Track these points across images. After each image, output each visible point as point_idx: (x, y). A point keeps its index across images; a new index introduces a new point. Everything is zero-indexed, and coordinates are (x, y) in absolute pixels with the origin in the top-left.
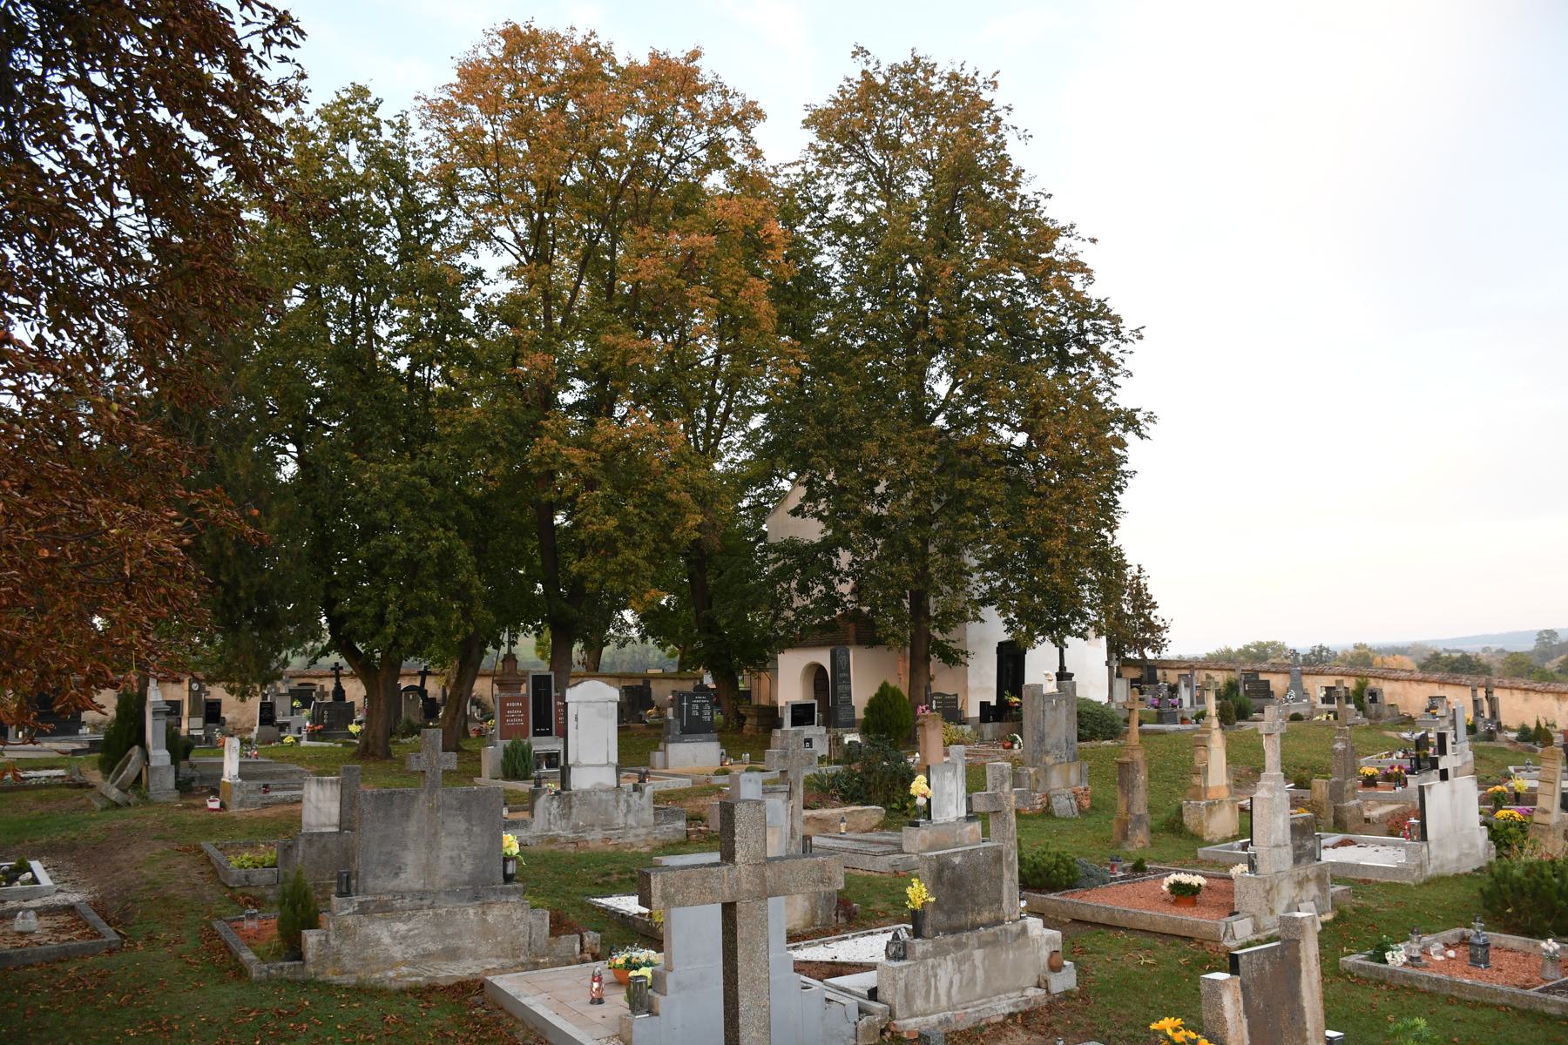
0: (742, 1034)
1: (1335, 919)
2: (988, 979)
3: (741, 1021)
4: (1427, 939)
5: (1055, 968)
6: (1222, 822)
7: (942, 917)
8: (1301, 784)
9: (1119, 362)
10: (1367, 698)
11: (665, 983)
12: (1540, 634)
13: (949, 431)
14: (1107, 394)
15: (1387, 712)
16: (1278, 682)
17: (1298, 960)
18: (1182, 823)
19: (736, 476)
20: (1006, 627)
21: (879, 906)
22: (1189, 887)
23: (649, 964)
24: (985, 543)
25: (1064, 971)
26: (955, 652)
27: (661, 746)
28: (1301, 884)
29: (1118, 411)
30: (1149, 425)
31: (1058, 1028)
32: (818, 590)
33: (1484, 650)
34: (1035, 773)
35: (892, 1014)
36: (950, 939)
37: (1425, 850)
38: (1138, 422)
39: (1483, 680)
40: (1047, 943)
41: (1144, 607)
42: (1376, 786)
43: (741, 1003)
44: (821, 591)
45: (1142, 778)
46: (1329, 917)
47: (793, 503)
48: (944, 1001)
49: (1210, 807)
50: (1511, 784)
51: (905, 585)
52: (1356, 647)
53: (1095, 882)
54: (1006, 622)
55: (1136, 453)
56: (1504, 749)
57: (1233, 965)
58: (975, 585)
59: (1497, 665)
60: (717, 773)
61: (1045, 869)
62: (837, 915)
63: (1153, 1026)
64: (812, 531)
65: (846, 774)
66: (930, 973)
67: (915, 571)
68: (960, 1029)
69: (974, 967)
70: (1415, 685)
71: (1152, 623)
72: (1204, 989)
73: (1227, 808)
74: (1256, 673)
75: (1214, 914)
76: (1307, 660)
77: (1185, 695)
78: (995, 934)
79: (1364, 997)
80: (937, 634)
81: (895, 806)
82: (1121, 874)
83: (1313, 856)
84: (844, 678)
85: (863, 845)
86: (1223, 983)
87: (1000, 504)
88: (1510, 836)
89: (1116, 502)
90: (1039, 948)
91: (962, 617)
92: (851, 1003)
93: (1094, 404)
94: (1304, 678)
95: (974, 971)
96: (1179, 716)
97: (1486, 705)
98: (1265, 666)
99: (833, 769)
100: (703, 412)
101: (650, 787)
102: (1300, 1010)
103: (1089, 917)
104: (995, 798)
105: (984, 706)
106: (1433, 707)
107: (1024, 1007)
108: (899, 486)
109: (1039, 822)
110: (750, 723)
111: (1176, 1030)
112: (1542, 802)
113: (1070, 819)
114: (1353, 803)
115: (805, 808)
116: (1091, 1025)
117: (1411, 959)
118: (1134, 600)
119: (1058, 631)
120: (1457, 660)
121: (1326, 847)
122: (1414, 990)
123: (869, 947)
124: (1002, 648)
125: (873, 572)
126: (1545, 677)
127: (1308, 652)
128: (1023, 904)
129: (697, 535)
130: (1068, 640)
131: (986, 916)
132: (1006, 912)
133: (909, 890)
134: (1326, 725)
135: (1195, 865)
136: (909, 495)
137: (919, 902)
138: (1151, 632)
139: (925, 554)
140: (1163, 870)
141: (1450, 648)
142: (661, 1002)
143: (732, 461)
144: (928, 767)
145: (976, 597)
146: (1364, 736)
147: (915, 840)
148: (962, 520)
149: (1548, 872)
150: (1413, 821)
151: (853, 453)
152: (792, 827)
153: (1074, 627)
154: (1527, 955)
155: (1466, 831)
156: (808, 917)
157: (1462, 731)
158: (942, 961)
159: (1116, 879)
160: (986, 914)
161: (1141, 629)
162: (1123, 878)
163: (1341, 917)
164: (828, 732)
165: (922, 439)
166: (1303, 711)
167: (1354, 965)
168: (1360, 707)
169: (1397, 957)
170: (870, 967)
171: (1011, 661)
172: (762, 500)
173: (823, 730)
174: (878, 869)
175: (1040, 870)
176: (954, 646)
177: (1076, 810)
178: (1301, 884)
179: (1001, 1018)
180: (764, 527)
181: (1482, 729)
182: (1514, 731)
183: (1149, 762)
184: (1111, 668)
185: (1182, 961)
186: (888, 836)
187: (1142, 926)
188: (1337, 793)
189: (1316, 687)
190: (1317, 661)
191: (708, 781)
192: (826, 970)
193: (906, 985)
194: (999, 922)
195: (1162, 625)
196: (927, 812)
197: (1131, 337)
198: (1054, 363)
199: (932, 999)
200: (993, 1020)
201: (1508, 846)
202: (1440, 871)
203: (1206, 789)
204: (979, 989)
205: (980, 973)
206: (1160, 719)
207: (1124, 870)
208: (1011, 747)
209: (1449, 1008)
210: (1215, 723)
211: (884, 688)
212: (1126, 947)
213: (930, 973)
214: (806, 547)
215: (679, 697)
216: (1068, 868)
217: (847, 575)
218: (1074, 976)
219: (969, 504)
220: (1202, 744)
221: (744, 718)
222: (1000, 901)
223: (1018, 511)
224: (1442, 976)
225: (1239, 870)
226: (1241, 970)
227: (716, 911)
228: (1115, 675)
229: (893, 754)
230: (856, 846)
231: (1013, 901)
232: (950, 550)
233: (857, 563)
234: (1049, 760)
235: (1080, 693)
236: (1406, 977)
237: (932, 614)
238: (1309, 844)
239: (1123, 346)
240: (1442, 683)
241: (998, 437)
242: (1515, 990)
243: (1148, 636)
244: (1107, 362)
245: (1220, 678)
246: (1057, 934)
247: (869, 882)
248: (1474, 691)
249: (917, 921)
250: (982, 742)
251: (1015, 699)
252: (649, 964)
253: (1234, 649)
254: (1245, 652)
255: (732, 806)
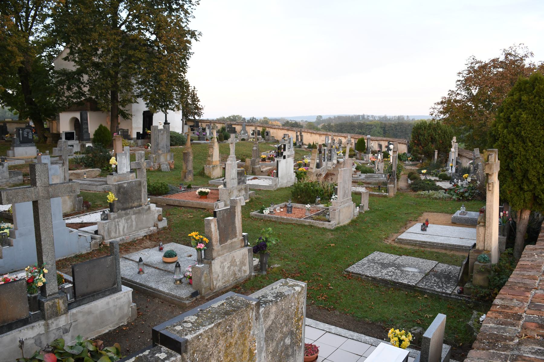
0: (43, 247)
1: (249, 201)
2: (137, 225)
3: (42, 243)
4: (275, 206)
5: (160, 220)
6: (217, 172)
7: (120, 205)
8: (243, 160)
9: (190, 12)
10: (265, 134)
11: (15, 234)
12: (318, 116)
13: (126, 32)
14: (186, 24)
15: (271, 139)
16: (238, 128)
17: (235, 212)
18: (204, 173)
19: (40, 43)
20: (146, 106)
21: (99, 203)
22: (205, 192)
23: (8, 228)
24: (139, 75)
25: (163, 221)
26: (127, 114)
27: (12, 148)
28: (240, 191)
29: (189, 31)
30: (199, 36)
31: (161, 239)
32: (75, 89)
33: (302, 121)
34: (155, 156)
35: (103, 239)
36: (123, 212)
37: (277, 180)
38: (196, 35)
39: (299, 130)
40: (157, 212)
41: (195, 101)
42: (265, 161)
43: (42, 237)
44: (76, 90)
45: (191, 158)
46: (248, 201)
47: (64, 55)
48: (122, 233)
49: (213, 167)
50: (304, 161)
51: (109, 88)
52: (264, 118)
53: (174, 192)
54: (146, 104)
55: (195, 46)
56: (303, 151)
57: (215, 214)
58: (135, 90)
59: (305, 126)
60: (36, 158)
61: (157, 188)
62: (83, 207)
63: (189, 235)
64: (72, 67)
65: (86, 158)
66: (117, 224)
67: (112, 83)
68: (128, 242)
69: (132, 221)
70: (280, 130)
71: (198, 107)
72: (205, 222)
73: (219, 168)
74: (231, 125)
75: (212, 201)
76: (248, 121)
77: (208, 131)
78: (139, 210)
79: (256, 224)
80: (121, 107)
81: (105, 168)
82: (183, 189)
83: (244, 182)
84: (85, 123)
85: (93, 182)
86: (211, 220)
87: (145, 60)
88: (302, 176)
89: (186, 63)
90: (155, 214)
91: (130, 101)
92: (88, 236)
93: (181, 27)
94: (246, 127)
95: (132, 223)
96: (205, 138)
97: (299, 137)
98: (235, 123)
99: (81, 156)
100: (24, 14)
101: (6, 164)
102: (235, 227)
103: (172, 203)
104: (138, 164)
105: (138, 134)
106: (284, 137)
107: (149, 233)
108: (106, 52)
109: (157, 173)
110: (49, 140)
111: (196, 236)
112: (311, 166)
113: (167, 172)
114: (258, 166)
115: (70, 170)
116: (172, 237)
117: (270, 212)
118: (192, 98)
119: (165, 108)
120: (294, 124)
121: (249, 180)
122: (270, 221)
123: (95, 217)
124: (145, 113)
125: (96, 83)
126: (318, 129)
127: (249, 119)
128: (149, 199)
129: (21, 65)
130: (168, 111)
131: (136, 204)
132: (143, 202)
133: (108, 196)
134: (253, 142)
135: (207, 186)
136: (110, 55)
137: (112, 200)
138: (197, 110)
139: (116, 77)
140: (197, 188)
141: (292, 120)
142: (14, 241)
143: (38, 36)
144: (116, 154)
145: (135, 94)
146: (263, 146)
147: (112, 180)
148: (130, 66)
149: (310, 186)
150: (275, 171)
151: (88, 37)
152: (65, 176)
153: (170, 107)
154: (302, 209)
155: (289, 174)
156: (72, 208)
157: (292, 144)
158: (121, 220)
159: (181, 191)
160: (136, 203)
161: (194, 109)
162: (184, 191)
163: (251, 201)
164: (79, 142)
165: (115, 34)
166: (246, 138)
167: (254, 214)
168: (263, 137)
169: (266, 212)
170: (94, 224)
171: (148, 118)
172: (52, 53)
173: (78, 142)
174: (98, 190)
175: (156, 189)
176: (127, 112)
177: (169, 169)
178: (240, 191)
179: (142, 237)
180: (53, 64)
181: (298, 145)
182: (306, 145)
183: (194, 153)
184: (183, 121)
185: (201, 216)
186: (102, 179)
187: (189, 205)
188: (253, 163)
189: (250, 130)
190: (252, 122)
191: (32, 161)
192: (79, 226)
193: (108, 229)
194: (141, 206)
195: (201, 107)
196: (116, 171)
197: (195, 4)
198: (167, 10)
199: (117, 232)
200: (139, 238)
201: (301, 179)
202: (281, 186)
203: (212, 161)
204: (134, 228)
205: (134, 223)
206: (199, 139)
207: (184, 188)
208: (148, 148)
209: (280, 225)
210: (216, 140)
211: (101, 126)
212: (184, 212)
213: (117, 224)
214: (70, 73)
215: (18, 130)
216: (165, 188)
217: (87, 84)
218: (166, 222)
219: (133, 60)
220: (211, 147)
221: (47, 138)
222: (141, 199)
223: (151, 64)
224: (278, 216)
225: (221, 187)
226: (217, 216)
227: (30, 204)
228: (185, 124)
229: (104, 150)
230: (90, 183)
231: (145, 199)
232: (125, 77)
233: (90, 79)
234: (160, 152)
235: (171, 130)
236: (269, 217)
237: (119, 100)
238: (243, 178)
239: (192, 7)
240: (288, 130)
241: (145, 35)
242: (298, 219)
243: (196, 111)
244: (186, 12)
245: (219, 126)
246: (161, 209)
247: (95, 195)
248: (297, 133)
249: (111, 207)
250: (137, 146)
251: (149, 131)
252: (8, 228)
253: (226, 117)
254: (229, 118)
255: (34, 165)
